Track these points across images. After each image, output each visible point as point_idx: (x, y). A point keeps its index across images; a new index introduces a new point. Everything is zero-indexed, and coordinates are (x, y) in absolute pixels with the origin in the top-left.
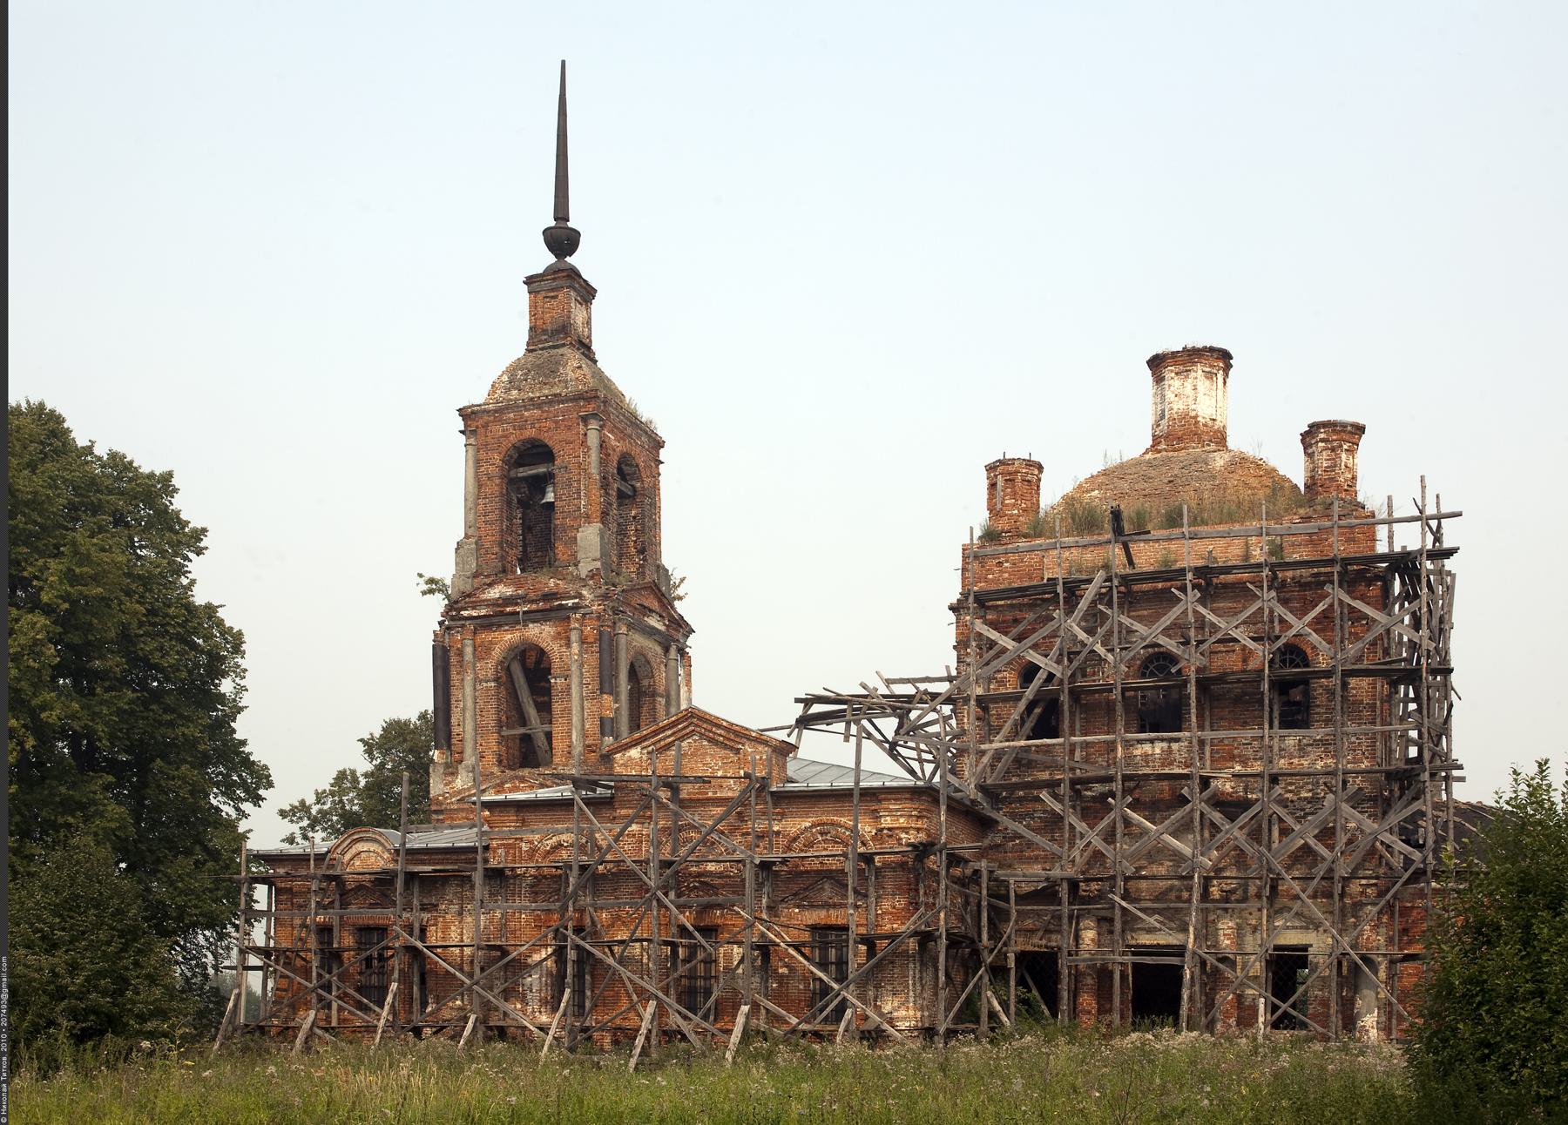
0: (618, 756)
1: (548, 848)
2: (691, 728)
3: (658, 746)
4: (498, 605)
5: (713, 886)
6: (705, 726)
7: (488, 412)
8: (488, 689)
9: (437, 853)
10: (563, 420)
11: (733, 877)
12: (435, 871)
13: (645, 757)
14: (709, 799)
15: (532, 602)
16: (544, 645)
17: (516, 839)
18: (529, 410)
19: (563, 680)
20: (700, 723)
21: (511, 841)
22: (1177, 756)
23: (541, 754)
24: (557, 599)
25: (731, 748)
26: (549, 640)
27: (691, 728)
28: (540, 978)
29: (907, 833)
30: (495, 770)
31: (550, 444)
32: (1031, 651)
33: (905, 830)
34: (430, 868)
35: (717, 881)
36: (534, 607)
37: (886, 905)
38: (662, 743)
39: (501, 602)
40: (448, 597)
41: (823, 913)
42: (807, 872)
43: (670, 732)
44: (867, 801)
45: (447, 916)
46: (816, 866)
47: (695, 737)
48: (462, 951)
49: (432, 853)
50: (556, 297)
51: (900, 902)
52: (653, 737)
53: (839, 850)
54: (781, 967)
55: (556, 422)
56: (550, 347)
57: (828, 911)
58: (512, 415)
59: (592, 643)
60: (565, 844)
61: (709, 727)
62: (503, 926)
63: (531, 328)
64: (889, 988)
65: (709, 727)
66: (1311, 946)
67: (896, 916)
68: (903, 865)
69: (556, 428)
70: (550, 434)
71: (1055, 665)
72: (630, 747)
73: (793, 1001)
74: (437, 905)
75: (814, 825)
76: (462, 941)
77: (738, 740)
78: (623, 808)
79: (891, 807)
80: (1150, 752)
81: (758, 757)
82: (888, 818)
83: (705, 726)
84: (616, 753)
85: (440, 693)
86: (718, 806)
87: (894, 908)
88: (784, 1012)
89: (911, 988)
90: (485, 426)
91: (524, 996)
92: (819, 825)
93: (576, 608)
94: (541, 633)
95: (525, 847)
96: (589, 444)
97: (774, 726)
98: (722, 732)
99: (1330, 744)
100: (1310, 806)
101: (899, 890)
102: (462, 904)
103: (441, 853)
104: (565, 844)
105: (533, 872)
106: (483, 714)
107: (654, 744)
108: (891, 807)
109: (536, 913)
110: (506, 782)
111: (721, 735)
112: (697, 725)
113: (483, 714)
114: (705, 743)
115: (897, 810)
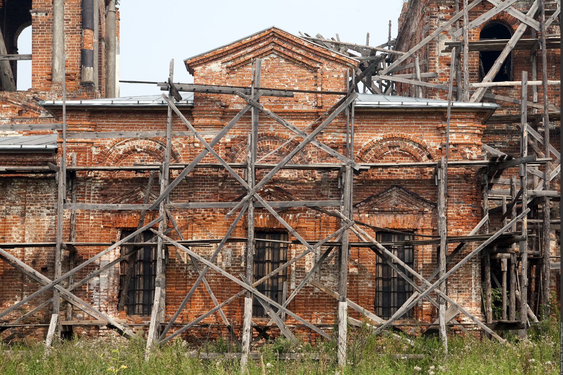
1: (121, 153)
2: (270, 47)
3: (238, 61)
5: (287, 193)
6: (285, 45)
9: (37, 154)
11: (306, 184)
12: (8, 172)
13: (224, 71)
14: (285, 112)
17: (87, 143)
19: (44, 15)
20: (280, 43)
21: (83, 145)
23: (5, 81)
25: (308, 67)
27: (270, 47)
28: (108, 278)
29: (470, 148)
32: (513, 9)
33: (469, 146)
35: (291, 188)
37: (452, 212)
38: (242, 59)
42: (378, 181)
43: (250, 50)
44: (433, 120)
45: (8, 216)
46: (385, 175)
47: (272, 56)
48: (23, 251)
49: (25, 155)
51: (464, 210)
52: (234, 53)
53: (408, 162)
54: (352, 267)
57: (395, 216)
60: (139, 150)
61: (289, 47)
62: (70, 228)
64: (455, 286)
65: (289, 47)
67: (461, 221)
68: (466, 177)
71: (534, 21)
72: (211, 61)
73: (363, 298)
75: (385, 140)
76: (24, 241)
77: (317, 59)
78: (200, 117)
79: (458, 125)
81: (336, 76)
82: (454, 135)
83: (285, 45)
84: (196, 66)
86: (293, 119)
87: (459, 214)
88: (362, 308)
89: (473, 286)
91: (90, 295)
92: (389, 139)
95: (95, 151)
97: (127, 83)
101: (463, 198)
102: (25, 205)
103: (42, 154)
104: (139, 150)
105: (103, 174)
107: (234, 59)
108: (458, 125)
109: (106, 214)
112: (276, 44)
114: (282, 61)
115: (463, 128)
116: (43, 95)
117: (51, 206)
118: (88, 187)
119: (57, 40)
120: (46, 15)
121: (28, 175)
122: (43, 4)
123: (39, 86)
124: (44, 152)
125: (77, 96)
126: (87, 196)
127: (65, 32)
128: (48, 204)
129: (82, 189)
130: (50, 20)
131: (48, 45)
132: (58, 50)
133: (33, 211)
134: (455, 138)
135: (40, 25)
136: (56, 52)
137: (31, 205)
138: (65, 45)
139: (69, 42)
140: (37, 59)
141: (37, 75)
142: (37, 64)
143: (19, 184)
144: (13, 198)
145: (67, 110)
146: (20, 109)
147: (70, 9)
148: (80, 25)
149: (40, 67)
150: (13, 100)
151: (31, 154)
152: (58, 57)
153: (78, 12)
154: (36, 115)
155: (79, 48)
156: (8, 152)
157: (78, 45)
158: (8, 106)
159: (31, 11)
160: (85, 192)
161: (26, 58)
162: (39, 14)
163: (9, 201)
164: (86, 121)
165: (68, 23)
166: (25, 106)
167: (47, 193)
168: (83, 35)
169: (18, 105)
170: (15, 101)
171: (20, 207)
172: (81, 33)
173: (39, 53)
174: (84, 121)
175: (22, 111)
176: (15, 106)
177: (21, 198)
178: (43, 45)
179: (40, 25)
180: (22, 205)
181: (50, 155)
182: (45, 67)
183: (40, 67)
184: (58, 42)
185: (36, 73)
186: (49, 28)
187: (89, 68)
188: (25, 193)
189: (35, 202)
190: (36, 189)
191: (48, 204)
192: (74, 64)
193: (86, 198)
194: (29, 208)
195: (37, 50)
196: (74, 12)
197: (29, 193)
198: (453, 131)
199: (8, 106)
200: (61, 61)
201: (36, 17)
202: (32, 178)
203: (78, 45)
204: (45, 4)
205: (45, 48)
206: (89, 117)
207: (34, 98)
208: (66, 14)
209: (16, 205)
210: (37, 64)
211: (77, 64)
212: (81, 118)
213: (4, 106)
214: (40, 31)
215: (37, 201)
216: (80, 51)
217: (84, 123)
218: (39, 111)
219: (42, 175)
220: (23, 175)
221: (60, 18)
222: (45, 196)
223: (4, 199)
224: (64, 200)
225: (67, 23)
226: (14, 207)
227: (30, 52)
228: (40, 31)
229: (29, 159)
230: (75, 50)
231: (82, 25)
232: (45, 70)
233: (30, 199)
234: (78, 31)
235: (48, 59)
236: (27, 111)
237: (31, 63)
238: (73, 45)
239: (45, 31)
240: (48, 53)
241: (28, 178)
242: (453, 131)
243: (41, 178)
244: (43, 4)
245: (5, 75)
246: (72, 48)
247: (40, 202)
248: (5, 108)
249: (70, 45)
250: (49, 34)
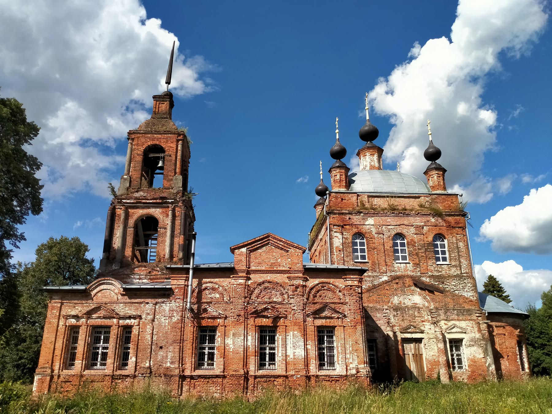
0: (236, 251)
22: (409, 269)
38: (256, 247)
41: (324, 321)
50: (164, 104)
55: (167, 140)
60: (208, 288)
61: (276, 241)
65: (276, 241)
66: (464, 338)
80: (400, 266)
82: (350, 281)
90: (138, 138)
94: (156, 212)
98: (282, 243)
99: (458, 267)
100: (455, 287)
111: (281, 245)
134: (350, 283)
198: (350, 279)
242: (350, 279)
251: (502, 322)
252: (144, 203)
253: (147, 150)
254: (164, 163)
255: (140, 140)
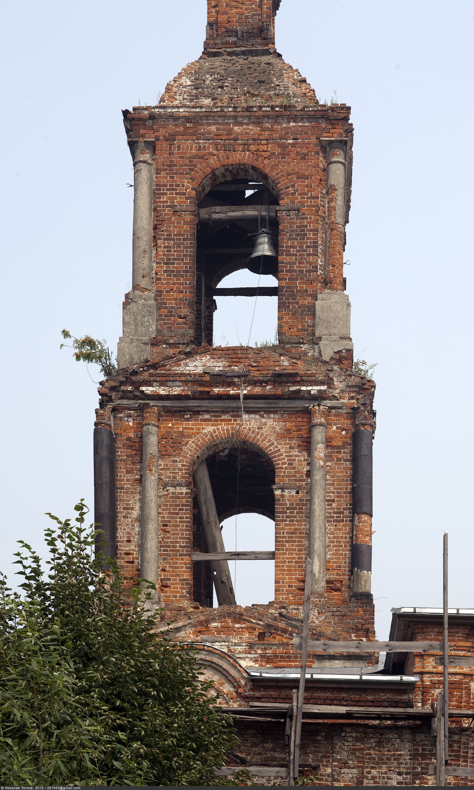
4: (202, 384)
7: (175, 118)
8: (175, 496)
9: (384, 690)
10: (293, 145)
12: (348, 715)
15: (255, 383)
16: (264, 444)
17: (465, 675)
18: (241, 124)
19: (293, 493)
24: (295, 383)
26: (273, 438)
30: (186, 604)
31: (273, 175)
34: (342, 710)
36: (257, 390)
39: (207, 378)
40: (107, 370)
49: (365, 690)
55: (284, 147)
56: (244, 53)
58: (213, 128)
59: (338, 447)
63: (210, 25)
69: (283, 155)
70: (273, 161)
74: (316, 768)
85: (364, 451)
90: (171, 139)
93: (320, 397)
96: (332, 181)
103: (391, 691)
106: (168, 528)
110: (214, 620)
113: (168, 528)
116: (295, 612)
117: (404, 771)
118: (464, 743)
119: (317, 530)
120: (297, 493)
121: (367, 722)
122: (292, 476)
123: (286, 599)
124: (397, 687)
125: (349, 613)
126: (464, 757)
127: (328, 519)
128: (399, 768)
129: (455, 745)
130: (302, 500)
131: (300, 537)
132: (317, 545)
133: (376, 777)
135: (288, 509)
136: (316, 548)
137: (372, 768)
138: (327, 539)
139: (333, 533)
140: (283, 558)
141: (283, 582)
142: (283, 566)
143: (354, 735)
144: (343, 755)
145: (449, 624)
146: (262, 631)
147: (334, 484)
148: (349, 509)
149: (288, 570)
150: (250, 617)
151: (375, 689)
152: (319, 556)
153: (347, 489)
154: (285, 641)
155: (348, 542)
156: (354, 686)
157: (346, 538)
158: (243, 626)
159: (274, 487)
160: (459, 751)
161: (264, 556)
162: (286, 491)
163: (339, 761)
164: (462, 641)
165: (331, 505)
166: (268, 626)
167: (397, 751)
168: (356, 523)
169: (259, 624)
170: (255, 618)
171: (355, 771)
172: (352, 521)
173: (287, 550)
174: (458, 640)
175: (264, 633)
176: (253, 625)
177: (357, 757)
178: (292, 537)
179: (288, 509)
180: (358, 767)
181: (404, 692)
182: (294, 571)
183: (288, 570)
184: (317, 534)
185: (280, 578)
186: (302, 513)
187: (365, 572)
188: (363, 749)
189: (378, 763)
190: (379, 744)
191: (399, 768)
192: (340, 567)
193: (462, 759)
194: (369, 773)
195: (282, 545)
196: (340, 489)
197: (369, 749)
199: (243, 626)
200: (322, 561)
201: (282, 496)
202: (374, 727)
203: (346, 538)
204: (296, 476)
205: (295, 542)
206: (467, 634)
207: (281, 614)
208: (328, 493)
209: (349, 768)
210: (283, 566)
211: (345, 567)
212: (455, 636)
213: (237, 626)
214: (287, 517)
215: (380, 762)
216: (349, 548)
217: (462, 644)
218: (291, 634)
219: (389, 722)
220: (359, 722)
221: (321, 497)
222: (395, 755)
223: (329, 757)
224: (446, 761)
225: (328, 505)
226: (346, 770)
227: (273, 549)
228: (287, 517)
229: (369, 698)
230: (341, 546)
231: (352, 509)
232: (296, 574)
233: (369, 758)
234: (347, 517)
235: (299, 558)
236: (272, 634)
237: (274, 564)
238: (338, 538)
239: (296, 517)
240: (299, 550)
241: (367, 726)
243: (388, 728)
244: (292, 476)
245: (223, 582)
246: (337, 542)
247: (386, 763)
248: (238, 628)
249: (334, 538)
250: (301, 521)
251: (153, 386)
252: (219, 397)
253: (208, 189)
254: (275, 244)
255: (179, 148)
